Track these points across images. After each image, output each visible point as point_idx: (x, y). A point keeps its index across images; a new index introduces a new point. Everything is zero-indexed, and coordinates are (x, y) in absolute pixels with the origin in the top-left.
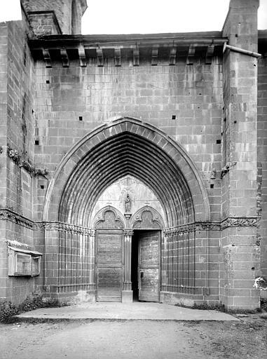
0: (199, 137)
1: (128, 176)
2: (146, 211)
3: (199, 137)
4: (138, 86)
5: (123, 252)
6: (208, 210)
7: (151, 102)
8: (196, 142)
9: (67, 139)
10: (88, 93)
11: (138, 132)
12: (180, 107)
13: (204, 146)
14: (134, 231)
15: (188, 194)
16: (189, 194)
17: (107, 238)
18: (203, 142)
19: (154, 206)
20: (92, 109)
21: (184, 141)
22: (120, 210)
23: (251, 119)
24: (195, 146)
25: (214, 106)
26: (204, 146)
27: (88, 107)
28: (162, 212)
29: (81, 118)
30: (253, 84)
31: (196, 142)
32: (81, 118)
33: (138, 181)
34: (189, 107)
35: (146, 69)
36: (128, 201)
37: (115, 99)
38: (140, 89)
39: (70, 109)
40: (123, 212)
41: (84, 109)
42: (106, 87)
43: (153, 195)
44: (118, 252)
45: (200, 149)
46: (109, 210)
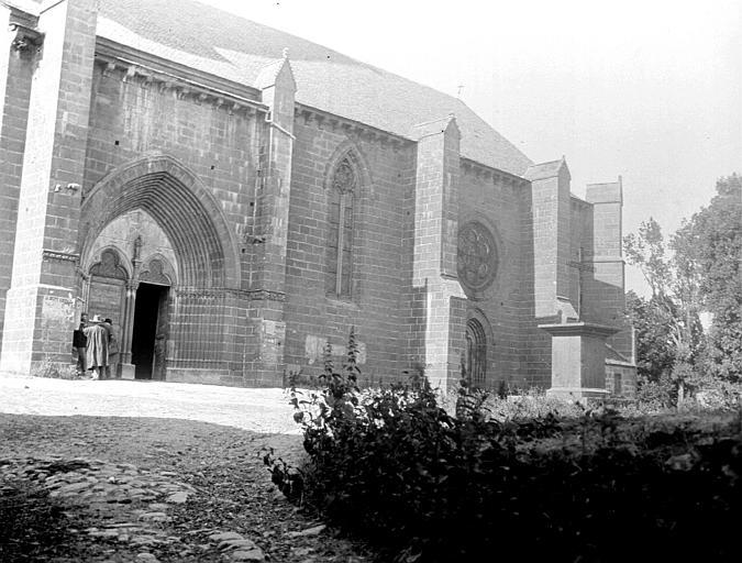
0: (235, 195)
1: (140, 210)
2: (157, 263)
3: (235, 195)
4: (181, 122)
5: (123, 311)
6: (239, 279)
7: (192, 145)
8: (232, 200)
9: (99, 164)
10: (127, 114)
11: (177, 175)
12: (415, 505)
13: (239, 206)
14: (141, 284)
15: (218, 254)
16: (221, 255)
17: (103, 289)
18: (238, 202)
19: (166, 255)
20: (130, 135)
21: (220, 195)
22: (126, 255)
23: (285, 196)
24: (232, 205)
25: (250, 166)
26: (239, 206)
27: (127, 131)
28: (175, 265)
29: (117, 143)
30: (288, 162)
31: (232, 200)
32: (117, 143)
33: (151, 219)
34: (227, 160)
35: (191, 105)
36: (137, 244)
37: (156, 130)
38: (183, 127)
39: (107, 129)
40: (130, 257)
41: (122, 132)
42: (147, 114)
43: (166, 240)
44: (116, 311)
45: (235, 208)
46: (111, 254)
